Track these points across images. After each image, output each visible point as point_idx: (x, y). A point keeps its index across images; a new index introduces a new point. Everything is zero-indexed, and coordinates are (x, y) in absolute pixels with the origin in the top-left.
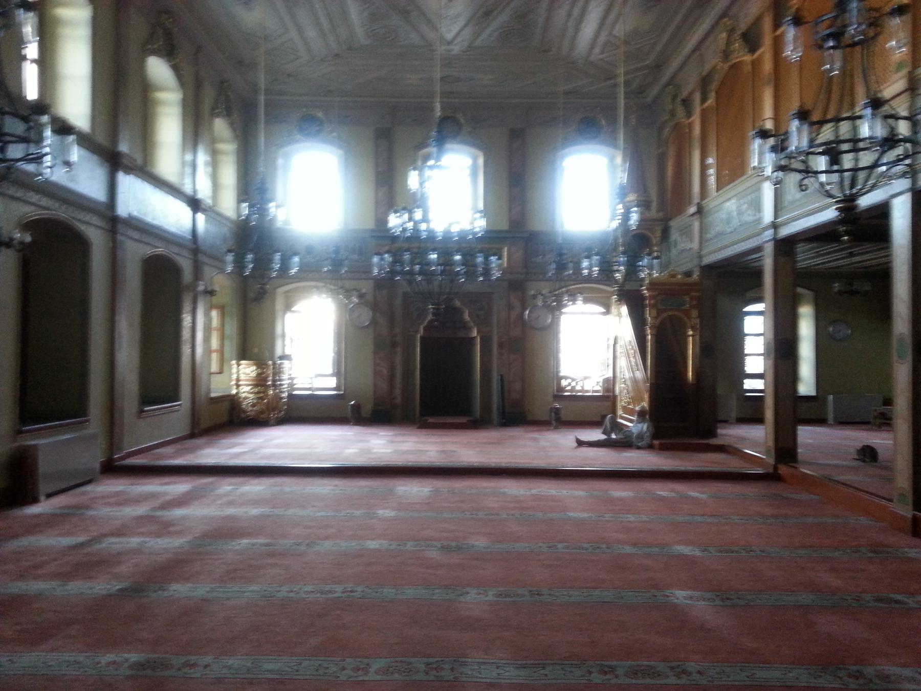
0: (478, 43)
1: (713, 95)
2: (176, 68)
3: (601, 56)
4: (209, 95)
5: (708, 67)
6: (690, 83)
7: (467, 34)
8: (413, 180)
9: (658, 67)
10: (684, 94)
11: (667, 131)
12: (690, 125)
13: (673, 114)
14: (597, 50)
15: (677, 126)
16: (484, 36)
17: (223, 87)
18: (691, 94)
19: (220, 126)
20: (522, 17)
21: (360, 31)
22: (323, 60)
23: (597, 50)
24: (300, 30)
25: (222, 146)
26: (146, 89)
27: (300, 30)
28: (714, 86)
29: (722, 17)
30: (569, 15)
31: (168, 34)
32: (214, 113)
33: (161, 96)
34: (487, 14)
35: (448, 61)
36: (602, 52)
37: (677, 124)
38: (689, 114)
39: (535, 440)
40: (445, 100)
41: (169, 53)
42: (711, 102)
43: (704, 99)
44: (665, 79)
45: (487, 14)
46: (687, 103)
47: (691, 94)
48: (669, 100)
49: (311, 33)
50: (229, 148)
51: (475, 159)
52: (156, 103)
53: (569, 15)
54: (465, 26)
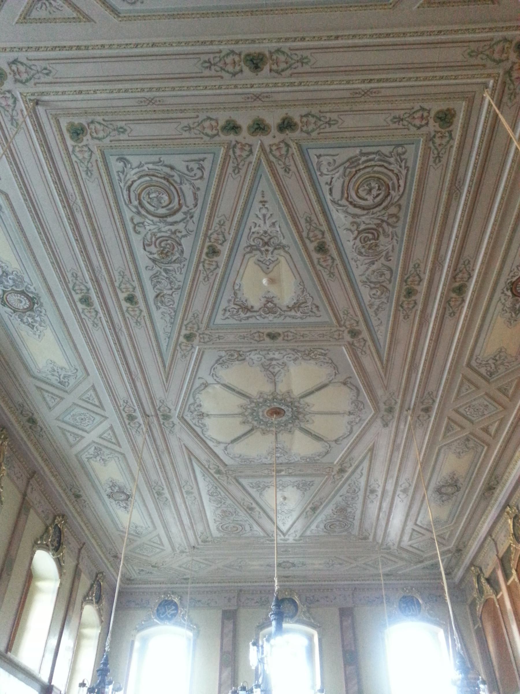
0: (308, 533)
1: (514, 572)
2: (59, 562)
3: (410, 543)
4: (84, 583)
5: (502, 550)
6: (490, 562)
7: (299, 526)
8: (253, 655)
9: (459, 551)
10: (487, 573)
11: (479, 608)
12: (501, 601)
13: (481, 591)
14: (406, 538)
15: (487, 602)
16: (313, 527)
17: (98, 579)
18: (494, 571)
19: (90, 612)
20: (342, 510)
21: (213, 526)
22: (182, 552)
23: (406, 538)
24: (166, 527)
25: (86, 631)
26: (30, 577)
27: (166, 527)
28: (514, 564)
29: (504, 507)
30: (380, 508)
31: (59, 532)
32: (85, 600)
33: (40, 584)
34: (314, 509)
35: (284, 549)
36: (410, 539)
37: (487, 601)
38: (497, 591)
39: (310, 650)
40: (281, 584)
41: (57, 548)
42: (514, 577)
43: (507, 576)
44: (467, 561)
45: (314, 509)
46: (492, 581)
47: (494, 571)
48: (475, 580)
49: (175, 530)
50: (93, 633)
51: (311, 638)
52: (37, 589)
53: (380, 508)
54: (298, 518)
